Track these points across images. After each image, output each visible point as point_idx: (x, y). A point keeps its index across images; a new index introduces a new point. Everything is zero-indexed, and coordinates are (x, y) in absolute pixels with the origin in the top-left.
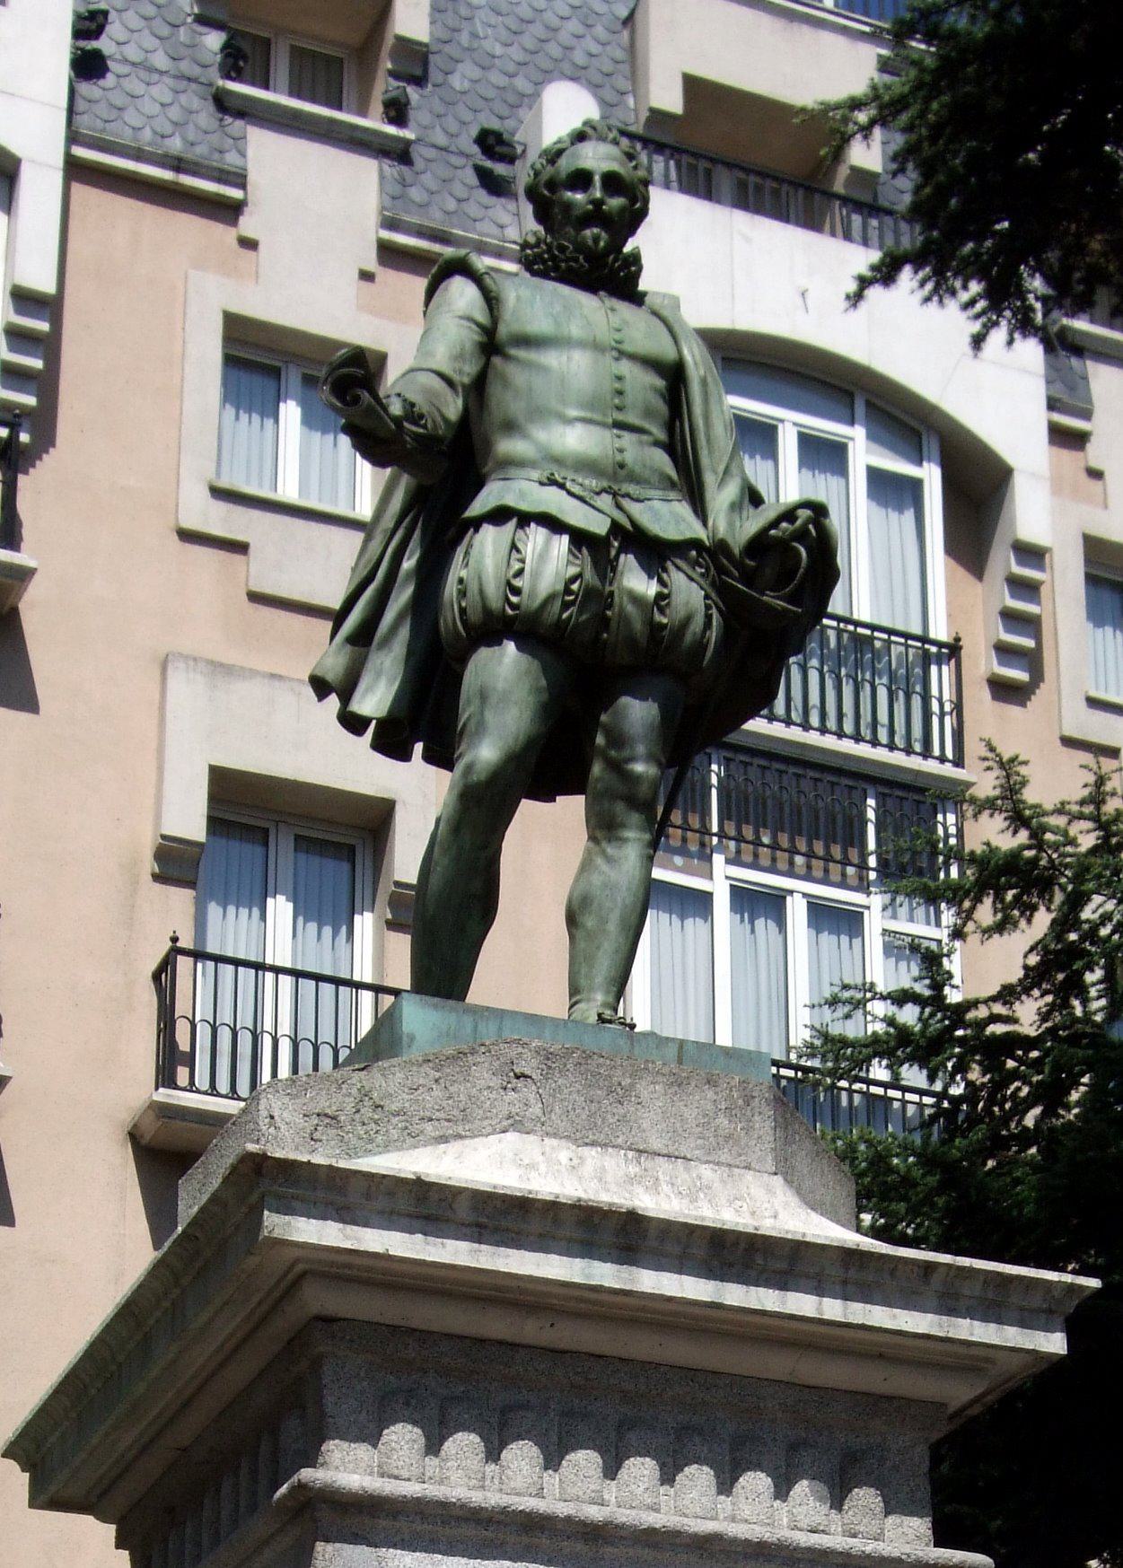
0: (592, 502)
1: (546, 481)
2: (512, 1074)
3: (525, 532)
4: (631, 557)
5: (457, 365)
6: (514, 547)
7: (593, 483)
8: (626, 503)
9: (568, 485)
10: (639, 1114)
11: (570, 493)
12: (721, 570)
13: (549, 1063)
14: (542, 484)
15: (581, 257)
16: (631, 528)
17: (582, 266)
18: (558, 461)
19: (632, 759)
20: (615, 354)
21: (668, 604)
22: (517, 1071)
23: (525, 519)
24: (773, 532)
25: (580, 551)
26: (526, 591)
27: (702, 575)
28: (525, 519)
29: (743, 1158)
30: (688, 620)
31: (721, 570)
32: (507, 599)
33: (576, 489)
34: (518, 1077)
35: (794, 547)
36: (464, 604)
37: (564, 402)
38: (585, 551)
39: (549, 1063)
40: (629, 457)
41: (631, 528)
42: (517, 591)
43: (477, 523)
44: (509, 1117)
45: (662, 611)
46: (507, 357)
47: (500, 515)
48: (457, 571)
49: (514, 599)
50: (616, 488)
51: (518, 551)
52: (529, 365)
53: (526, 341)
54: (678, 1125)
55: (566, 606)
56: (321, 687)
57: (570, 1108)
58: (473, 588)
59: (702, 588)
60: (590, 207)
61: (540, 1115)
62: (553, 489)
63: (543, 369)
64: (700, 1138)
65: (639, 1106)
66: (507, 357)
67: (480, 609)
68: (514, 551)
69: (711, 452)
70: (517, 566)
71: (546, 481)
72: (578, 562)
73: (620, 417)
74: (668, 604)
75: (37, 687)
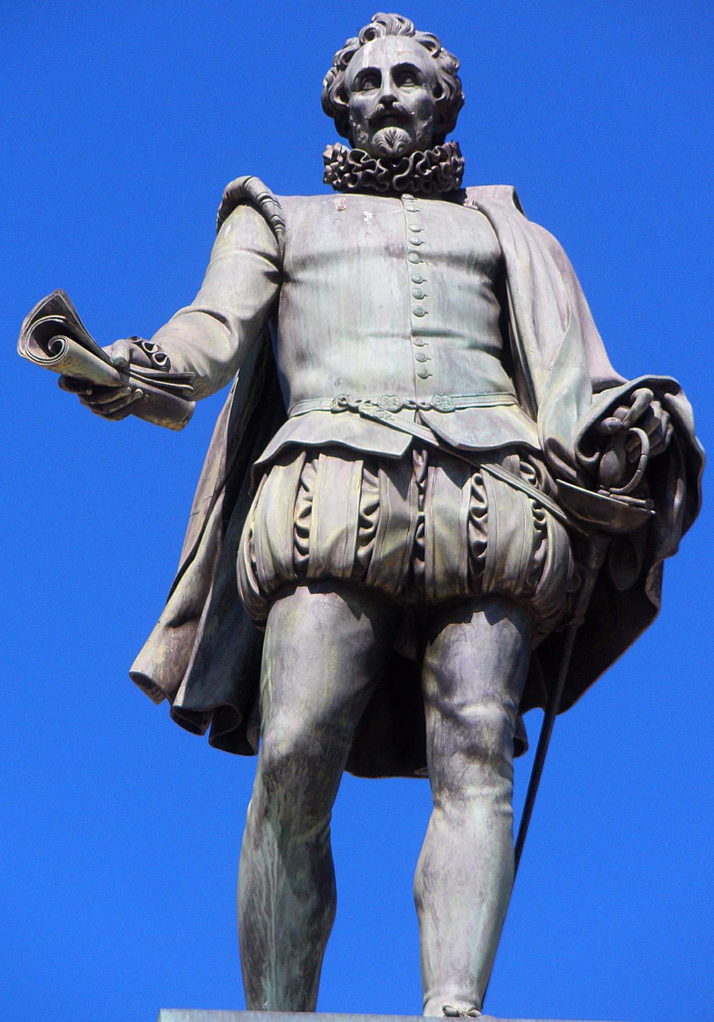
4: (441, 471)
6: (301, 484)
8: (428, 415)
11: (364, 416)
12: (555, 473)
14: (334, 412)
16: (437, 444)
17: (380, 171)
20: (414, 257)
21: (486, 521)
23: (312, 452)
24: (608, 421)
25: (376, 475)
27: (533, 482)
28: (312, 452)
31: (555, 473)
32: (296, 544)
33: (371, 411)
35: (633, 432)
36: (254, 560)
38: (382, 473)
41: (437, 444)
42: (304, 533)
43: (266, 468)
46: (295, 282)
47: (288, 453)
48: (251, 522)
49: (303, 542)
50: (419, 401)
51: (307, 489)
52: (314, 286)
53: (304, 263)
55: (363, 541)
58: (261, 542)
59: (530, 497)
60: (381, 106)
66: (295, 282)
67: (270, 564)
68: (302, 488)
70: (303, 506)
72: (376, 490)
73: (419, 323)
74: (486, 521)
75: (336, 873)
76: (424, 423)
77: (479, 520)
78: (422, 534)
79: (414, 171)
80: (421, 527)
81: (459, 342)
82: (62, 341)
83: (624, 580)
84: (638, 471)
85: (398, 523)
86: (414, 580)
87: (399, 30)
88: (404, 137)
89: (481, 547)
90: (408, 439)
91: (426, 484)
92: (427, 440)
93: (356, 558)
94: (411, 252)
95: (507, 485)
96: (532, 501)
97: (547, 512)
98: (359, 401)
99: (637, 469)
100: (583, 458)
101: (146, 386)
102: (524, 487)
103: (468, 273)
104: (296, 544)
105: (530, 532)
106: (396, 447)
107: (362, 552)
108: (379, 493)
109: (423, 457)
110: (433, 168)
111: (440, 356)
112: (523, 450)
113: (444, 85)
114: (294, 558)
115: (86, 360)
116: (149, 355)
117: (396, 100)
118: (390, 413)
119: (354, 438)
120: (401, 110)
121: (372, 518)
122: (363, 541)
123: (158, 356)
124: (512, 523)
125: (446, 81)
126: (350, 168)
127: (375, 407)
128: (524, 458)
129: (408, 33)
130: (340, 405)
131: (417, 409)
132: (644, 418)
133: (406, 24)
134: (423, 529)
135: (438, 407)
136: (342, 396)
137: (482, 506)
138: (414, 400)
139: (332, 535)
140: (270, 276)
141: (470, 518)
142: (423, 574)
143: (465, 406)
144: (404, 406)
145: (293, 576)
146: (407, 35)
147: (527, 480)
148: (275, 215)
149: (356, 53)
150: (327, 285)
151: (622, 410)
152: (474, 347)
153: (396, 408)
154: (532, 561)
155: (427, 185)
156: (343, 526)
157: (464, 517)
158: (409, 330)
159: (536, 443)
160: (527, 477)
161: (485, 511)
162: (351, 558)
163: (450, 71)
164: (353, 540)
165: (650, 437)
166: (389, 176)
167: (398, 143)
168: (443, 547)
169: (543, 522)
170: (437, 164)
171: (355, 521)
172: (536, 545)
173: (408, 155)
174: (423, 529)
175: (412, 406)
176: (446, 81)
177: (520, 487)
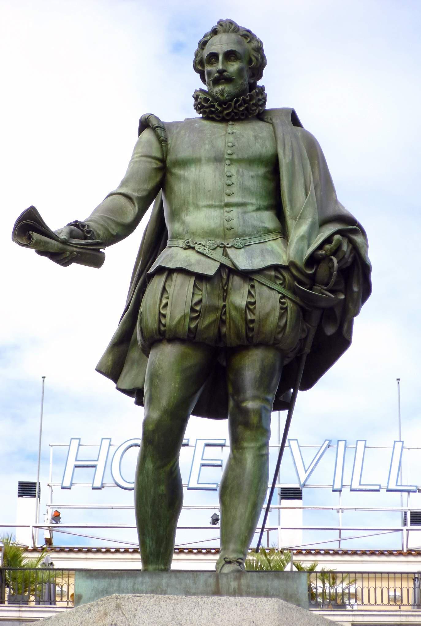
1: (185, 247)
3: (244, 284)
6: (164, 290)
7: (211, 243)
9: (197, 247)
14: (185, 249)
15: (216, 104)
17: (217, 109)
20: (228, 162)
23: (171, 271)
26: (256, 329)
30: (268, 315)
33: (201, 249)
40: (234, 223)
45: (252, 311)
47: (161, 270)
55: (192, 319)
56: (413, 579)
59: (279, 293)
62: (190, 252)
69: (292, 208)
70: (164, 301)
72: (201, 293)
73: (227, 200)
74: (255, 308)
77: (252, 307)
78: (225, 314)
79: (235, 108)
81: (250, 208)
82: (32, 234)
83: (330, 331)
84: (332, 280)
85: (213, 309)
86: (220, 336)
87: (230, 29)
88: (229, 91)
89: (252, 321)
90: (218, 265)
92: (228, 265)
93: (189, 329)
94: (227, 159)
96: (280, 295)
98: (196, 243)
99: (332, 279)
102: (277, 288)
103: (258, 167)
104: (160, 321)
105: (277, 312)
106: (210, 269)
107: (193, 326)
109: (226, 273)
110: (245, 106)
111: (238, 217)
113: (253, 58)
115: (46, 243)
116: (83, 231)
118: (210, 250)
119: (191, 265)
120: (64, 240)
121: (198, 308)
122: (192, 319)
123: (87, 231)
124: (268, 309)
127: (203, 247)
129: (235, 30)
132: (336, 251)
133: (234, 25)
134: (225, 311)
135: (235, 246)
136: (188, 240)
137: (253, 301)
139: (178, 317)
141: (247, 306)
142: (225, 335)
143: (250, 244)
144: (218, 246)
145: (157, 337)
146: (234, 32)
147: (278, 284)
148: (162, 137)
149: (209, 42)
150: (184, 178)
151: (327, 247)
152: (258, 209)
153: (213, 247)
154: (278, 326)
155: (243, 115)
156: (183, 314)
160: (279, 282)
161: (254, 303)
162: (187, 329)
163: (257, 50)
164: (188, 319)
165: (338, 262)
166: (222, 112)
167: (226, 95)
169: (285, 306)
170: (247, 103)
171: (188, 310)
174: (225, 311)
176: (254, 56)
177: (274, 288)
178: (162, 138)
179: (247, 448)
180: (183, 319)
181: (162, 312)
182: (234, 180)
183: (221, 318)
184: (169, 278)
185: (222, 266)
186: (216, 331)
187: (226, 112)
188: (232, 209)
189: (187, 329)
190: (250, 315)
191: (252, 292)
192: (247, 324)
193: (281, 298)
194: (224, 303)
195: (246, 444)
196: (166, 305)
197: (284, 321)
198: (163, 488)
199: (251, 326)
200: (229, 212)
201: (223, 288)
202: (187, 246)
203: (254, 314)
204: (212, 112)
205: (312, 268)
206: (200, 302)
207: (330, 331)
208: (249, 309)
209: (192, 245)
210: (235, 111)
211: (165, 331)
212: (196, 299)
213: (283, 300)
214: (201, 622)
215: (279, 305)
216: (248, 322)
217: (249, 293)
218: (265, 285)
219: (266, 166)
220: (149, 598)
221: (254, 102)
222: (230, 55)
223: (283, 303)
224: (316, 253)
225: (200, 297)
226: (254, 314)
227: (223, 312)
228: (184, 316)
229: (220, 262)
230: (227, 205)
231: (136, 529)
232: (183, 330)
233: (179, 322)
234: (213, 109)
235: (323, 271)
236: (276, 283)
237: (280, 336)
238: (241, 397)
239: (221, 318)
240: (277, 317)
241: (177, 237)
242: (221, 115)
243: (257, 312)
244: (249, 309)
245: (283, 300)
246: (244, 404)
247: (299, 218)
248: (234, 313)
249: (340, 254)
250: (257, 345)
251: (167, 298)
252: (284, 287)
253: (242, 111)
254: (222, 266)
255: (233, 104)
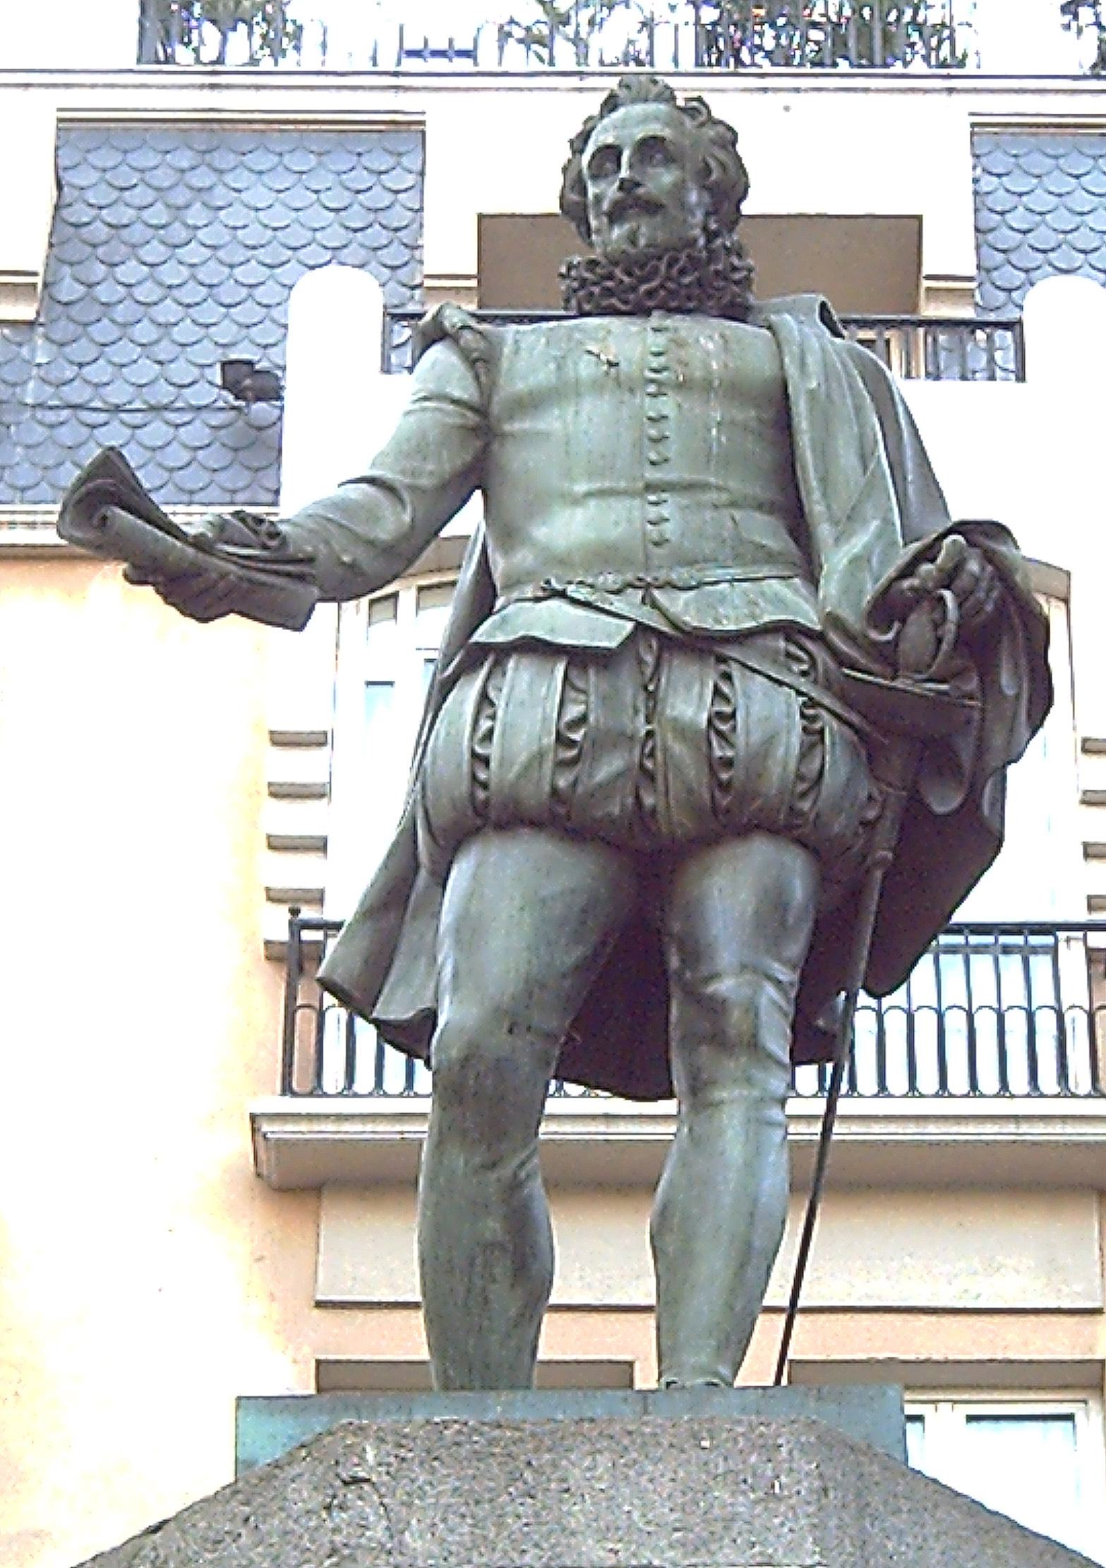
0: (607, 607)
2: (338, 1483)
5: (408, 465)
9: (571, 590)
10: (565, 1508)
11: (575, 602)
13: (402, 1452)
14: (537, 600)
18: (563, 561)
19: (714, 976)
22: (344, 1476)
24: (906, 584)
27: (804, 674)
29: (757, 1549)
30: (769, 742)
32: (474, 777)
33: (582, 594)
34: (345, 1483)
37: (568, 475)
39: (402, 1452)
42: (486, 761)
44: (333, 1552)
54: (636, 1515)
57: (437, 1520)
59: (799, 693)
61: (383, 1540)
62: (555, 604)
63: (545, 436)
64: (676, 1530)
65: (566, 1496)
70: (485, 724)
71: (540, 594)
73: (652, 475)
74: (734, 728)
76: (655, 605)
77: (724, 727)
78: (652, 755)
80: (650, 744)
83: (944, 801)
89: (728, 763)
91: (657, 687)
93: (555, 791)
95: (765, 680)
97: (824, 713)
100: (874, 635)
101: (242, 572)
104: (474, 777)
107: (562, 783)
108: (587, 703)
110: (696, 274)
112: (790, 630)
113: (713, 164)
114: (472, 795)
117: (638, 185)
121: (577, 736)
122: (562, 764)
125: (716, 159)
126: (584, 283)
128: (788, 639)
130: (544, 589)
131: (648, 587)
134: (653, 749)
137: (727, 709)
138: (641, 575)
140: (475, 430)
151: (926, 567)
157: (704, 723)
158: (640, 485)
159: (812, 620)
160: (796, 668)
164: (548, 765)
165: (960, 606)
166: (634, 289)
168: (679, 770)
169: (817, 726)
172: (804, 755)
173: (660, 258)
175: (638, 583)
178: (475, 355)
179: (722, 1102)
180: (536, 764)
181: (479, 750)
182: (669, 429)
183: (642, 766)
184: (498, 670)
185: (640, 628)
186: (630, 801)
187: (644, 288)
188: (664, 496)
189: (547, 788)
190: (721, 748)
191: (725, 689)
192: (713, 772)
193: (804, 704)
194: (649, 727)
195: (722, 1094)
196: (489, 735)
197: (816, 764)
198: (493, 1227)
199: (724, 776)
200: (656, 504)
201: (646, 688)
202: (544, 589)
203: (732, 746)
204: (609, 292)
205: (889, 628)
206: (582, 720)
207: (944, 801)
208: (720, 734)
209: (558, 587)
210: (671, 285)
211: (486, 803)
212: (573, 711)
213: (810, 712)
214: (592, 1488)
215: (798, 722)
216: (715, 766)
217: (717, 692)
218: (759, 672)
219: (758, 407)
220: (441, 1428)
221: (720, 267)
222: (649, 148)
223: (813, 719)
224: (892, 591)
225: (582, 708)
226: (732, 746)
227: (647, 750)
228: (540, 756)
229: (630, 619)
230: (650, 487)
231: (418, 1318)
232: (535, 794)
233: (527, 767)
234: (610, 284)
235: (918, 627)
236: (790, 670)
237: (806, 805)
238: (704, 971)
239: (642, 766)
240: (796, 750)
241: (513, 583)
242: (631, 297)
243: (740, 739)
244: (720, 734)
245: (810, 712)
246: (712, 988)
247: (850, 520)
248: (677, 748)
249: (963, 581)
250: (745, 831)
251: (493, 717)
252: (815, 682)
253: (687, 286)
254: (640, 628)
255: (663, 268)
